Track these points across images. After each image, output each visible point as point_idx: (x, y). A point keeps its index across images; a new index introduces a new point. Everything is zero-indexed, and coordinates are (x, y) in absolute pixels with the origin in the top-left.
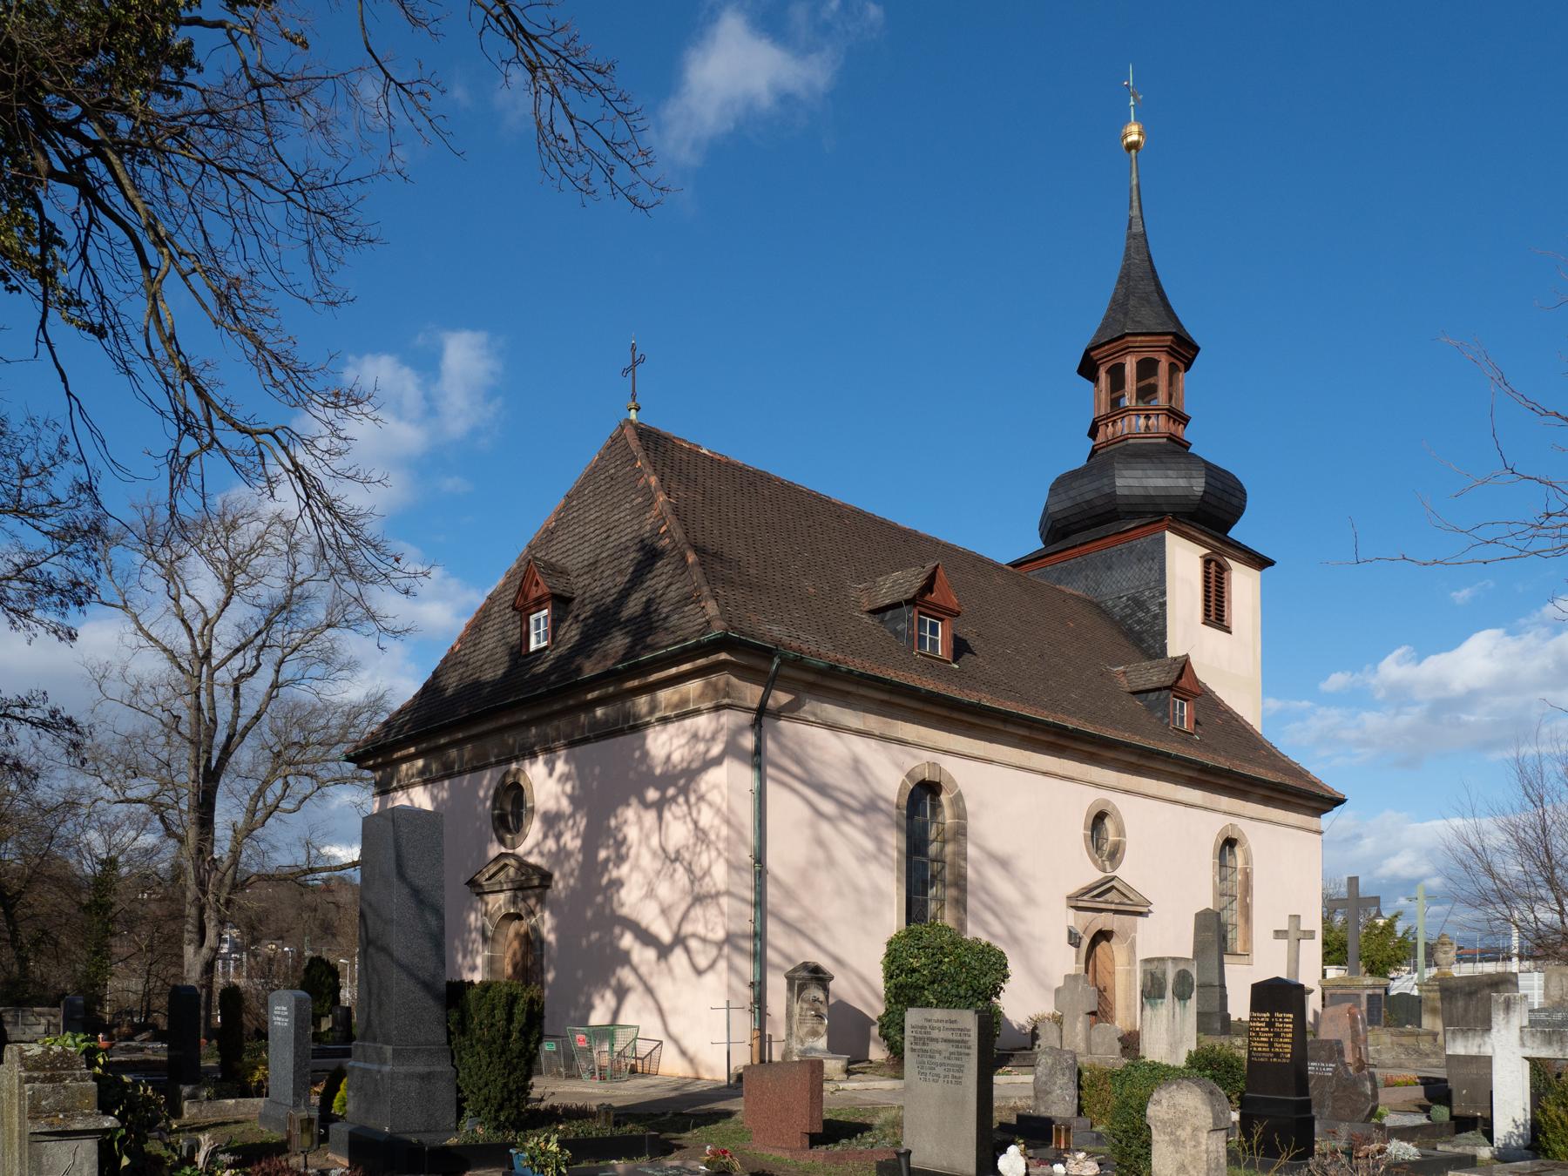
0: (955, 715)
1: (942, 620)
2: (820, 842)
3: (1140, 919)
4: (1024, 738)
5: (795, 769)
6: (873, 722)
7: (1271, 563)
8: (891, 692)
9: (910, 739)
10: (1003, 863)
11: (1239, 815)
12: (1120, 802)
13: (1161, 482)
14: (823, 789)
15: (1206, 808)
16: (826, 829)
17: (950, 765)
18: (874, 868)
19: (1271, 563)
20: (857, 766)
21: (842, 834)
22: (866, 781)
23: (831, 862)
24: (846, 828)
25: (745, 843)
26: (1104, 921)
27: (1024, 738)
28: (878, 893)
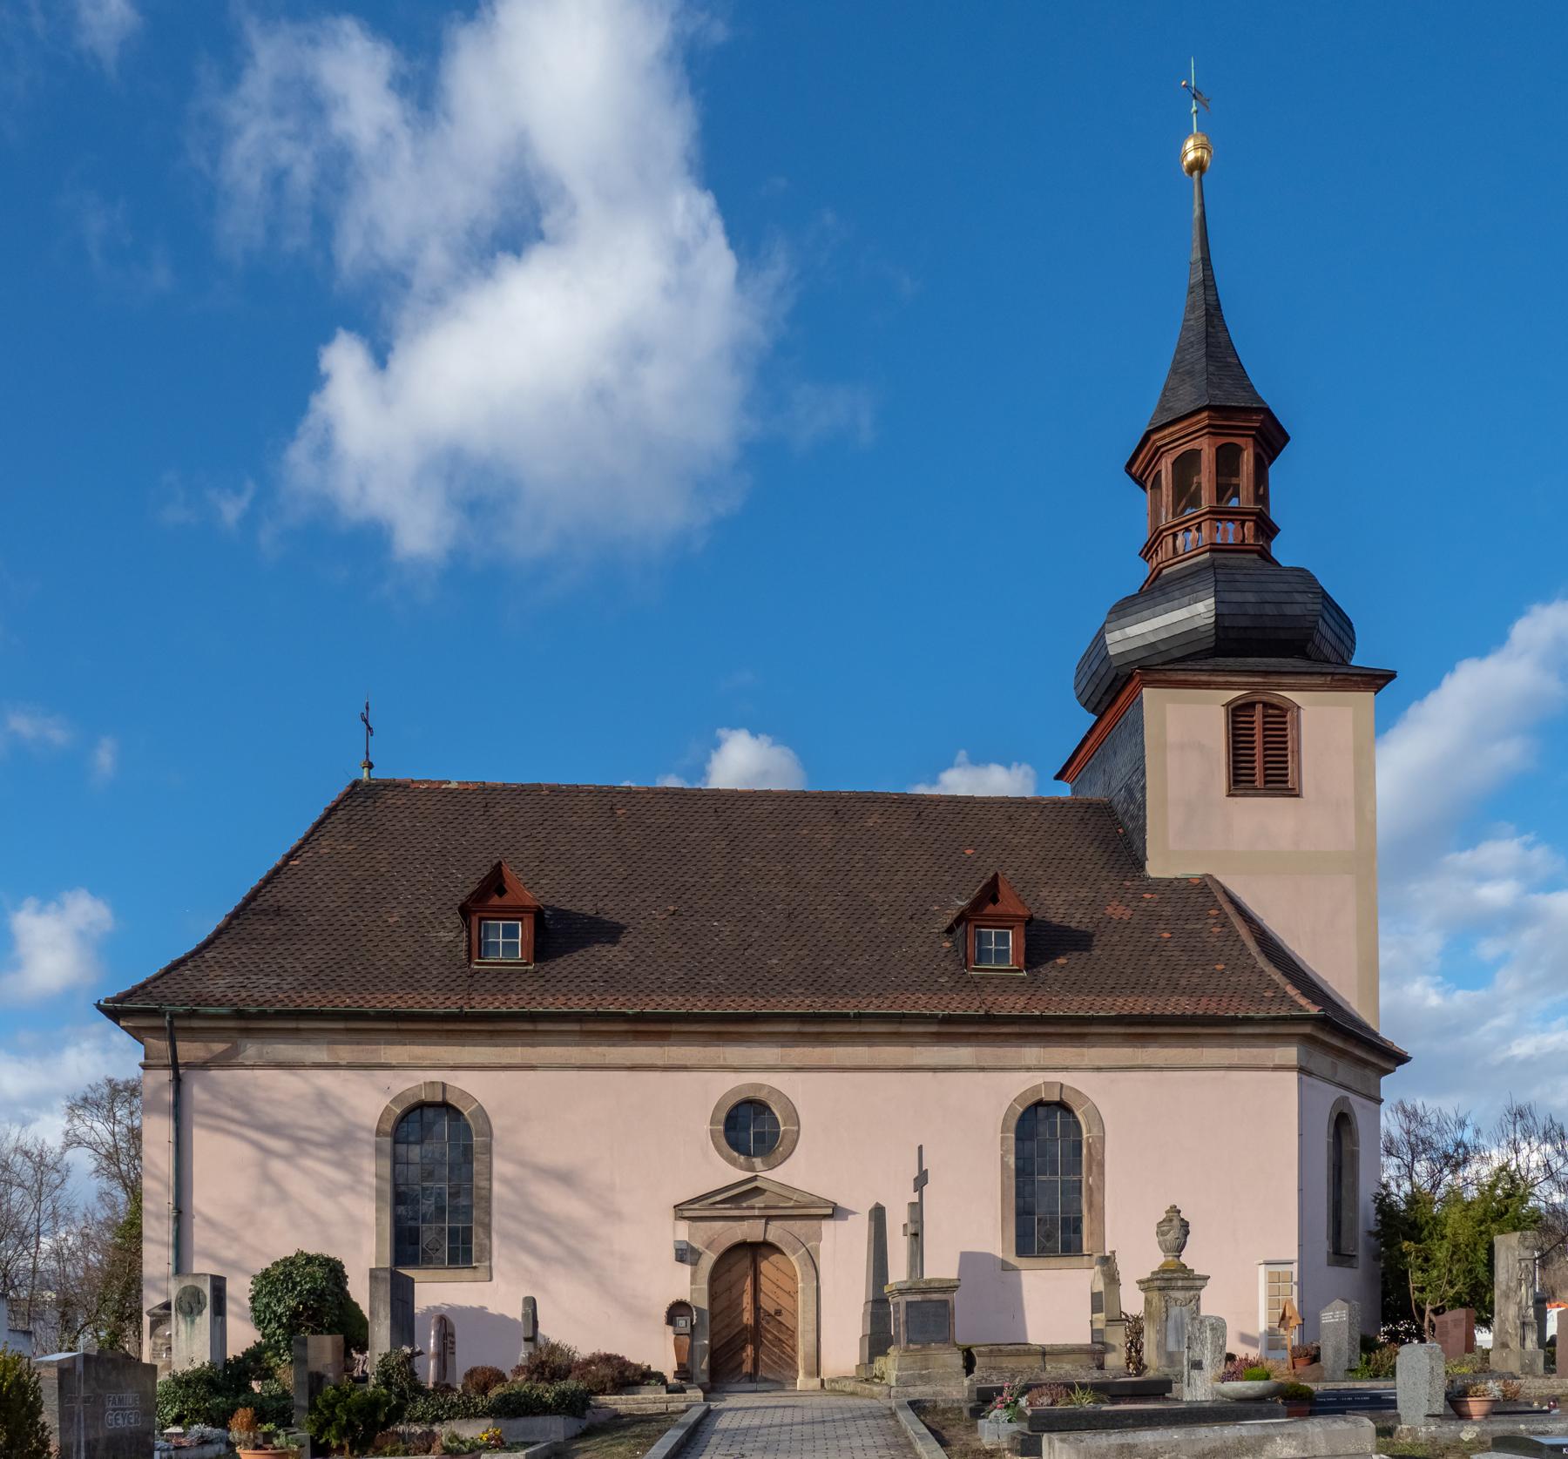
0: (302, 1025)
1: (520, 919)
2: (267, 1178)
3: (827, 1226)
4: (582, 1033)
5: (237, 1114)
6: (346, 1053)
7: (1389, 676)
8: (1073, 1025)
9: (394, 1062)
10: (565, 1178)
11: (1066, 1069)
12: (484, 1081)
13: (1133, 631)
14: (274, 1129)
15: (982, 1069)
16: (277, 1166)
17: (463, 1082)
18: (348, 1201)
19: (1389, 676)
20: (322, 1100)
21: (305, 1172)
22: (339, 1114)
23: (283, 1196)
24: (309, 1163)
25: (506, 1181)
26: (750, 1231)
27: (582, 1033)
28: (353, 1222)
